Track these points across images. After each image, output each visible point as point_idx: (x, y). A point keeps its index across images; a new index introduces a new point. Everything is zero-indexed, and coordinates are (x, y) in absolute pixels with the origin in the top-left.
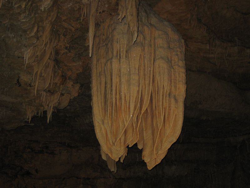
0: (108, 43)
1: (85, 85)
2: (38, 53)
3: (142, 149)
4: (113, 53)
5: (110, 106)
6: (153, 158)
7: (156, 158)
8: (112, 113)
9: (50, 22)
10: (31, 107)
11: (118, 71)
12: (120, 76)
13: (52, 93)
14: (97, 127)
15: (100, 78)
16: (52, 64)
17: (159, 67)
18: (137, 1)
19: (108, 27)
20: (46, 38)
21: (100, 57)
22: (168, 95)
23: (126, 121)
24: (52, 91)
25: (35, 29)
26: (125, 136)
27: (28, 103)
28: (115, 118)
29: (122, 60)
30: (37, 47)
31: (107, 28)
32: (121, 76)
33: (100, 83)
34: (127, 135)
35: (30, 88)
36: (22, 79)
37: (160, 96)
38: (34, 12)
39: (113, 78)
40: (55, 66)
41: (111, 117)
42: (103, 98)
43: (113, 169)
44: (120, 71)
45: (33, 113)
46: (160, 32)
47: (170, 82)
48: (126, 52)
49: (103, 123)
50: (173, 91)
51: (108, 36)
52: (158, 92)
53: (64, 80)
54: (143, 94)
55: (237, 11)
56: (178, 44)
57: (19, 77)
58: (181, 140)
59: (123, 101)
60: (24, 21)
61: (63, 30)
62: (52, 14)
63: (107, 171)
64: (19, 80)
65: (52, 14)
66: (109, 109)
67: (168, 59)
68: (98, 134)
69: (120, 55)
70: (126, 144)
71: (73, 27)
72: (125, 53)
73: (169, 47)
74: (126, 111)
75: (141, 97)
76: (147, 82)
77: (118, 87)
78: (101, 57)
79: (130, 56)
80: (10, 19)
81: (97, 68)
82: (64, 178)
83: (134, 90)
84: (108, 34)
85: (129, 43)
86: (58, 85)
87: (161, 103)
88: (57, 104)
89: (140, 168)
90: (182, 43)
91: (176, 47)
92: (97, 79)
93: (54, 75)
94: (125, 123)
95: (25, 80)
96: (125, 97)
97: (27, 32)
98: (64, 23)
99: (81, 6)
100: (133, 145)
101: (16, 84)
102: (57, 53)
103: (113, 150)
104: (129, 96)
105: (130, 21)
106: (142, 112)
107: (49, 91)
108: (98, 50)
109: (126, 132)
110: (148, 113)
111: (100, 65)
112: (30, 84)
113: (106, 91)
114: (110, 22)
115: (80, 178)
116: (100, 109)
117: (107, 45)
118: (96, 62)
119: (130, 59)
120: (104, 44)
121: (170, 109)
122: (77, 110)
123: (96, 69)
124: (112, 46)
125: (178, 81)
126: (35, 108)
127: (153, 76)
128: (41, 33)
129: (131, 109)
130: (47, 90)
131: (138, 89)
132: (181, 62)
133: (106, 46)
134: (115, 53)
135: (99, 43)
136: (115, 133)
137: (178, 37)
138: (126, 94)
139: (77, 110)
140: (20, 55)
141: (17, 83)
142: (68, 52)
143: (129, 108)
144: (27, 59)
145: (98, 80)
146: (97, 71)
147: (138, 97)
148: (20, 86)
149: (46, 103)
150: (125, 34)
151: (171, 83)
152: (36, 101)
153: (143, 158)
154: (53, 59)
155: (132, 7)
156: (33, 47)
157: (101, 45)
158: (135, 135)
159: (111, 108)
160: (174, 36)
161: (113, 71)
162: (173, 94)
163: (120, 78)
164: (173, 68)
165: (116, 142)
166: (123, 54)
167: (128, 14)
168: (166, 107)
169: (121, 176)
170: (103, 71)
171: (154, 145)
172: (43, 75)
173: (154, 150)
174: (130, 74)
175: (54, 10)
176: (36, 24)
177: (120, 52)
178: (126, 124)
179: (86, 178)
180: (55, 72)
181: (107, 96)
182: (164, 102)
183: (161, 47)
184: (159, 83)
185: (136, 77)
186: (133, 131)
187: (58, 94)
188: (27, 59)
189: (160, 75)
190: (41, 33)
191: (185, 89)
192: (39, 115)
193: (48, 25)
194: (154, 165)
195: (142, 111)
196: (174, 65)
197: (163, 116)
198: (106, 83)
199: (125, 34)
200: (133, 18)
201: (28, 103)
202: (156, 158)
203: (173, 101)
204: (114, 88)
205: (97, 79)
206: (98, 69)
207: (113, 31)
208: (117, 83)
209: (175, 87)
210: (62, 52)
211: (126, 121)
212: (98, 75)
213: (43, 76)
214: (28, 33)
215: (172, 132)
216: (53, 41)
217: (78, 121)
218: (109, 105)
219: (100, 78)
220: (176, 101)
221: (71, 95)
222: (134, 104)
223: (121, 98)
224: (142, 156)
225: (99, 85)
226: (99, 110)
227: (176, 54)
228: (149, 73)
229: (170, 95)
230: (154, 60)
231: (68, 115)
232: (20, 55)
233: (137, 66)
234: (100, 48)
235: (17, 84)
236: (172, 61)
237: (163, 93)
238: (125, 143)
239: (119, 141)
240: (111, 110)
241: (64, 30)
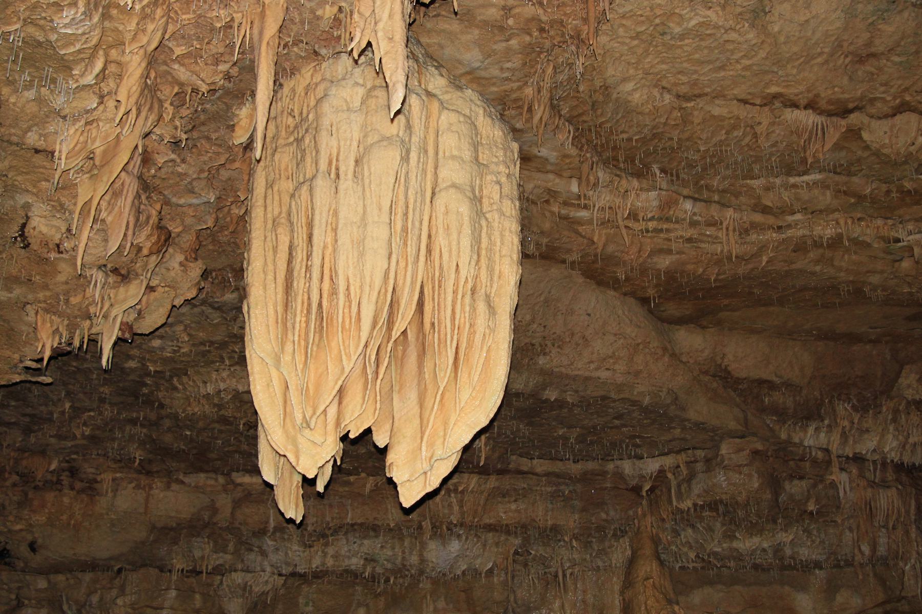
0: (303, 137)
1: (214, 274)
2: (97, 144)
3: (386, 447)
4: (316, 164)
5: (302, 311)
6: (417, 470)
7: (425, 473)
8: (307, 334)
9: (142, 52)
10: (53, 317)
11: (331, 212)
12: (335, 230)
13: (123, 276)
14: (257, 376)
15: (276, 235)
16: (131, 186)
17: (447, 213)
18: (406, 2)
19: (307, 89)
20: (129, 97)
21: (277, 176)
22: (469, 292)
23: (349, 357)
24: (123, 272)
25: (99, 65)
26: (340, 403)
27: (43, 305)
28: (315, 349)
29: (343, 185)
30: (95, 125)
31: (303, 94)
32: (340, 226)
33: (275, 250)
34: (344, 403)
35: (58, 256)
36: (34, 228)
37: (445, 293)
38: (101, 10)
39: (316, 232)
40: (140, 197)
41: (303, 343)
42: (280, 289)
43: (292, 507)
44: (336, 213)
45: (57, 339)
46: (453, 117)
47: (475, 257)
48: (357, 161)
49: (278, 361)
50: (484, 281)
51: (304, 115)
52: (440, 281)
53: (163, 238)
54: (400, 282)
55: (663, 88)
56: (501, 153)
57: (28, 218)
58: (483, 459)
59: (342, 297)
60: (69, 31)
61: (173, 87)
62: (151, 27)
63: (257, 549)
64: (26, 230)
65: (151, 27)
66: (298, 319)
67: (473, 191)
68: (260, 394)
69: (337, 169)
70: (343, 426)
71: (203, 81)
72: (352, 163)
73: (477, 159)
74: (350, 328)
75: (387, 307)
76: (411, 250)
77: (327, 260)
78: (280, 175)
79: (366, 174)
80: (25, 20)
81: (266, 207)
82: (120, 571)
83: (375, 265)
84: (305, 111)
85: (365, 136)
86: (145, 252)
87: (449, 312)
88: (133, 316)
89: (355, 543)
90: (512, 152)
91: (495, 160)
92: (266, 238)
93: (137, 220)
94: (345, 362)
95: (44, 229)
96: (348, 289)
97: (71, 69)
98: (176, 66)
99: (234, 15)
100: (361, 431)
101: (16, 238)
102: (146, 159)
103: (296, 447)
104: (358, 284)
105: (386, 53)
106: (396, 333)
107: (115, 271)
108: (273, 155)
109: (341, 392)
110: (408, 340)
111: (276, 198)
112: (58, 246)
113: (292, 271)
114: (312, 76)
115: (170, 571)
116: (270, 323)
117: (299, 141)
118: (263, 190)
119: (367, 181)
120: (292, 139)
121: (475, 332)
122: (182, 351)
123: (263, 209)
124: (315, 142)
125: (497, 255)
126: (66, 322)
127: (430, 236)
128: (112, 84)
129: (363, 321)
130: (109, 266)
131: (386, 266)
132: (509, 202)
133: (295, 144)
134: (323, 166)
135: (275, 137)
136: (311, 392)
137: (501, 133)
138: (351, 281)
139: (182, 351)
140: (42, 142)
141: (20, 236)
142: (178, 161)
143: (359, 319)
144: (63, 157)
145: (269, 239)
146: (265, 214)
147: (386, 291)
148: (26, 246)
149: (101, 308)
150: (356, 111)
151: (478, 261)
152: (72, 299)
153: (387, 471)
154: (135, 172)
155: (391, 16)
156: (83, 122)
157: (281, 142)
158: (371, 398)
159: (304, 319)
160: (492, 131)
161: (317, 212)
162: (483, 291)
163: (336, 235)
164: (487, 219)
165: (316, 417)
166: (347, 167)
167: (380, 34)
168: (462, 326)
169: (296, 565)
170: (284, 215)
171: (423, 433)
172: (103, 215)
173: (424, 448)
174: (363, 222)
175: (157, 17)
176: (101, 52)
177: (337, 160)
178: (346, 366)
179: (187, 571)
180: (139, 212)
181: (295, 284)
182: (458, 311)
183: (453, 157)
184: (445, 256)
185: (384, 233)
186: (366, 388)
187: (142, 281)
188: (63, 157)
189: (448, 235)
190: (112, 84)
191: (518, 277)
192: (77, 343)
193: (137, 59)
194: (419, 492)
195: (394, 333)
196: (490, 211)
197: (454, 350)
198: (291, 248)
199: (356, 111)
200: (393, 47)
201: (43, 305)
202: (425, 473)
203: (481, 306)
204: (316, 260)
205: (266, 238)
206: (269, 209)
207: (319, 101)
208: (325, 247)
209: (490, 270)
210: (160, 160)
211: (349, 357)
212: (270, 225)
213: (103, 221)
214: (77, 72)
215: (475, 400)
216: (143, 114)
217: (180, 387)
218: (299, 308)
219: (276, 235)
220: (492, 310)
221: (175, 290)
222: (372, 307)
223: (334, 292)
224: (387, 464)
225: (271, 252)
226: (268, 326)
227: (495, 179)
228: (417, 224)
229: (473, 291)
230: (433, 194)
231: (152, 368)
232: (42, 142)
233: (386, 204)
234: (279, 150)
235: (19, 239)
236: (484, 200)
237: (456, 284)
238: (338, 424)
239: (322, 416)
240: (304, 325)
241: (176, 90)
